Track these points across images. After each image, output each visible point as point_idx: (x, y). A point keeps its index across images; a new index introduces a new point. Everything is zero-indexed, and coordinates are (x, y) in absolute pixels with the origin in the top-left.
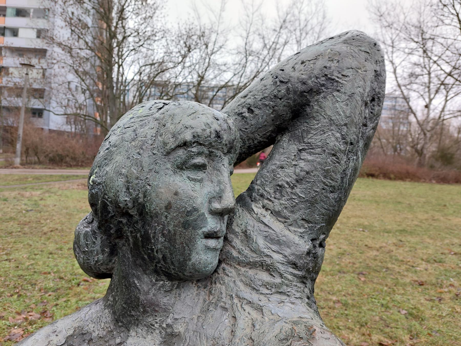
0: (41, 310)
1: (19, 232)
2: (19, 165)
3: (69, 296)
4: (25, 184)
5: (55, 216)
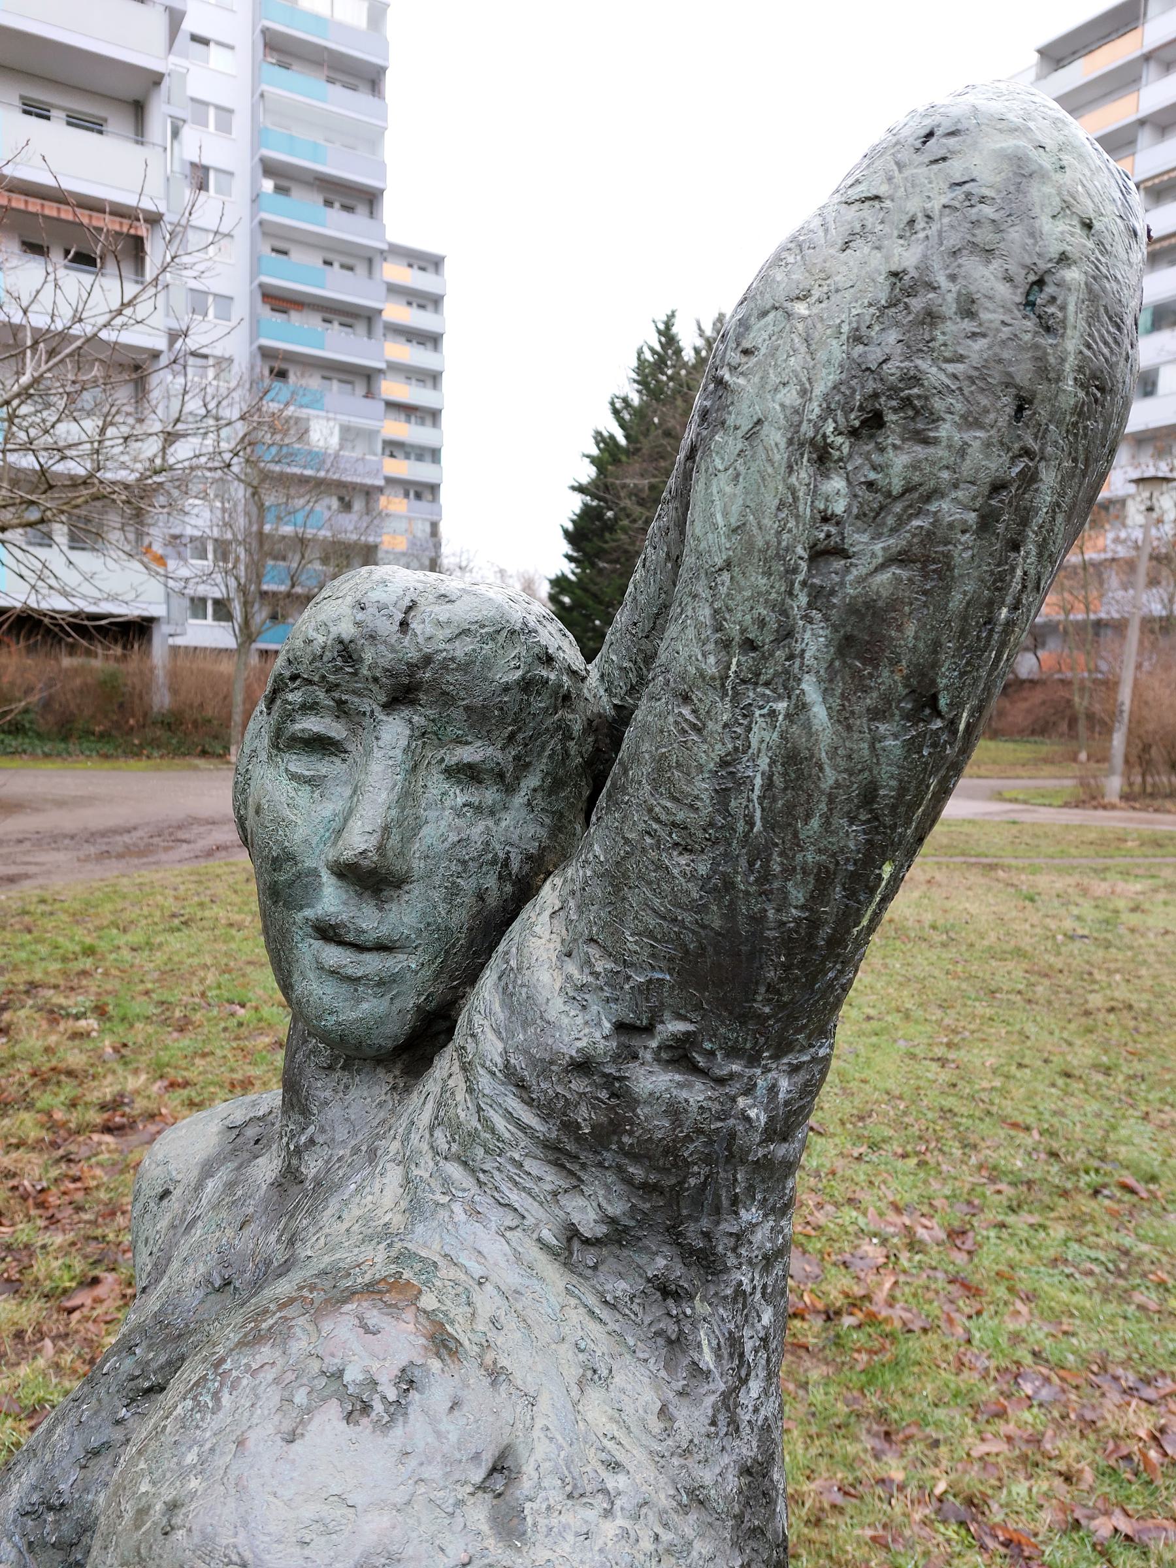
0: (956, 1224)
1: (1019, 992)
2: (1115, 800)
3: (1052, 1215)
4: (1111, 857)
5: (1149, 966)
